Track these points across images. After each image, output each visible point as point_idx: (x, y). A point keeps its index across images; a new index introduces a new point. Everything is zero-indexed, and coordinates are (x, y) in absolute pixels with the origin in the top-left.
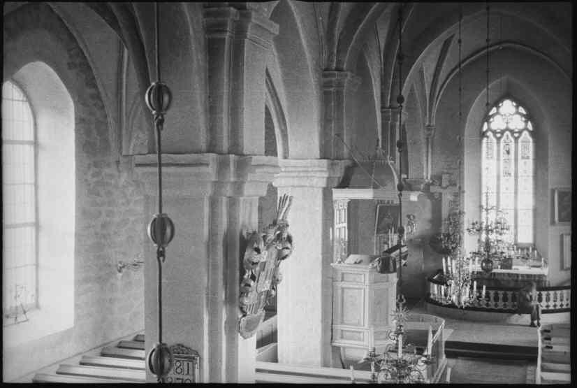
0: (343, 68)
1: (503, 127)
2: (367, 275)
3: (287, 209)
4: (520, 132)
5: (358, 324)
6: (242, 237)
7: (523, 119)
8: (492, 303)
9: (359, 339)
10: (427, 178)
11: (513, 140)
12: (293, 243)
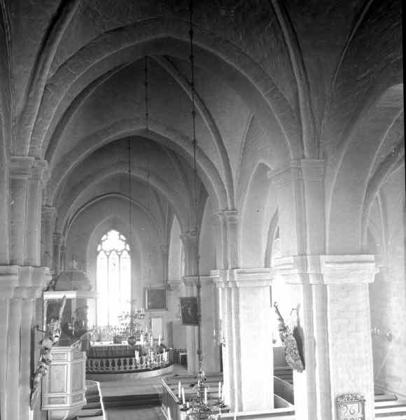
2: (69, 354)
4: (122, 251)
5: (63, 391)
7: (124, 243)
9: (64, 403)
10: (222, 289)
11: (118, 257)
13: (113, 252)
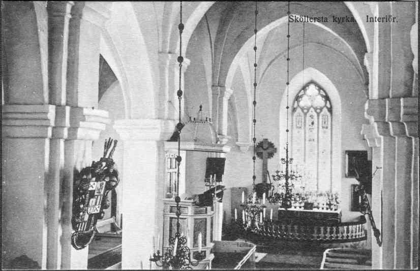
0: (166, 51)
1: (309, 104)
3: (112, 151)
4: (321, 109)
6: (76, 171)
7: (324, 99)
8: (328, 235)
12: (119, 177)
13: (312, 109)
